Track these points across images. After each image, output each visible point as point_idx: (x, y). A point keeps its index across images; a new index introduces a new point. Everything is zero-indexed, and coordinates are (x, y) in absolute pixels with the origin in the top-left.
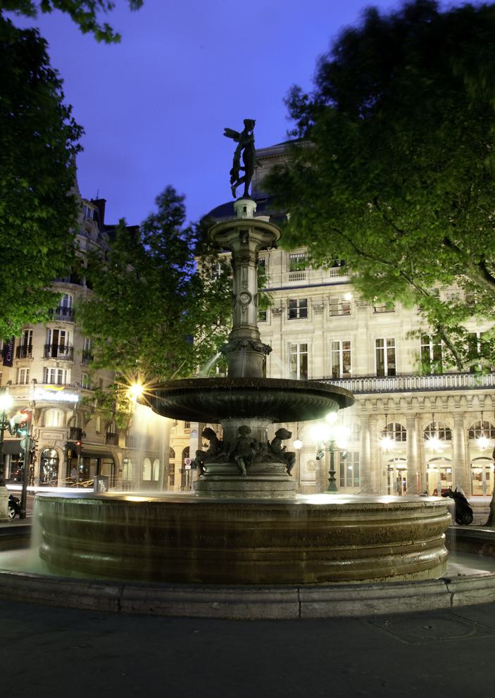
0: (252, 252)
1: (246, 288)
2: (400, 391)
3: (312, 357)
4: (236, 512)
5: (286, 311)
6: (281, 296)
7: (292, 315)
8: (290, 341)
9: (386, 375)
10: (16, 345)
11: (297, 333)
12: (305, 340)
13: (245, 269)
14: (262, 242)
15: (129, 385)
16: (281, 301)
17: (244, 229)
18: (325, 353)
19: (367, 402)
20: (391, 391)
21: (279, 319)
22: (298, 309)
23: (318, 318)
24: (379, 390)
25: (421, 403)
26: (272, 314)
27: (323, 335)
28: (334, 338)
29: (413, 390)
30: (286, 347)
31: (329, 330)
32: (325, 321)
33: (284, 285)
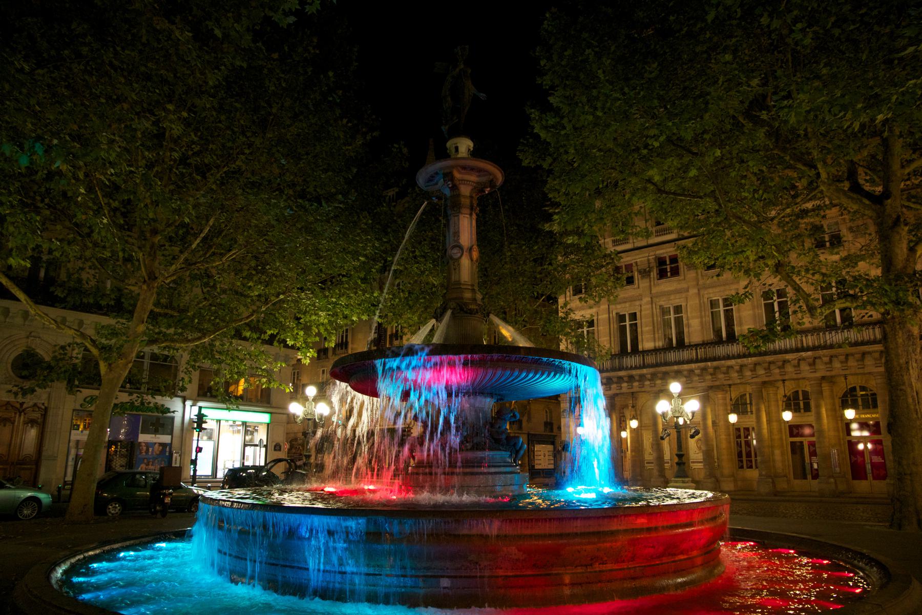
0: (465, 197)
1: (458, 241)
2: (797, 350)
3: (688, 319)
4: (623, 518)
5: (655, 270)
6: (647, 255)
7: (662, 275)
8: (662, 303)
9: (629, 350)
10: (389, 333)
11: (669, 293)
12: (677, 301)
13: (456, 218)
14: (477, 183)
15: (174, 412)
16: (648, 260)
17: (448, 171)
18: (703, 313)
19: (772, 367)
20: (786, 351)
21: (648, 280)
22: (668, 267)
23: (691, 274)
24: (719, 357)
25: (826, 363)
26: (640, 276)
27: (699, 294)
28: (711, 295)
29: (814, 348)
30: (658, 310)
31: (706, 287)
32: (700, 276)
33: (651, 241)
